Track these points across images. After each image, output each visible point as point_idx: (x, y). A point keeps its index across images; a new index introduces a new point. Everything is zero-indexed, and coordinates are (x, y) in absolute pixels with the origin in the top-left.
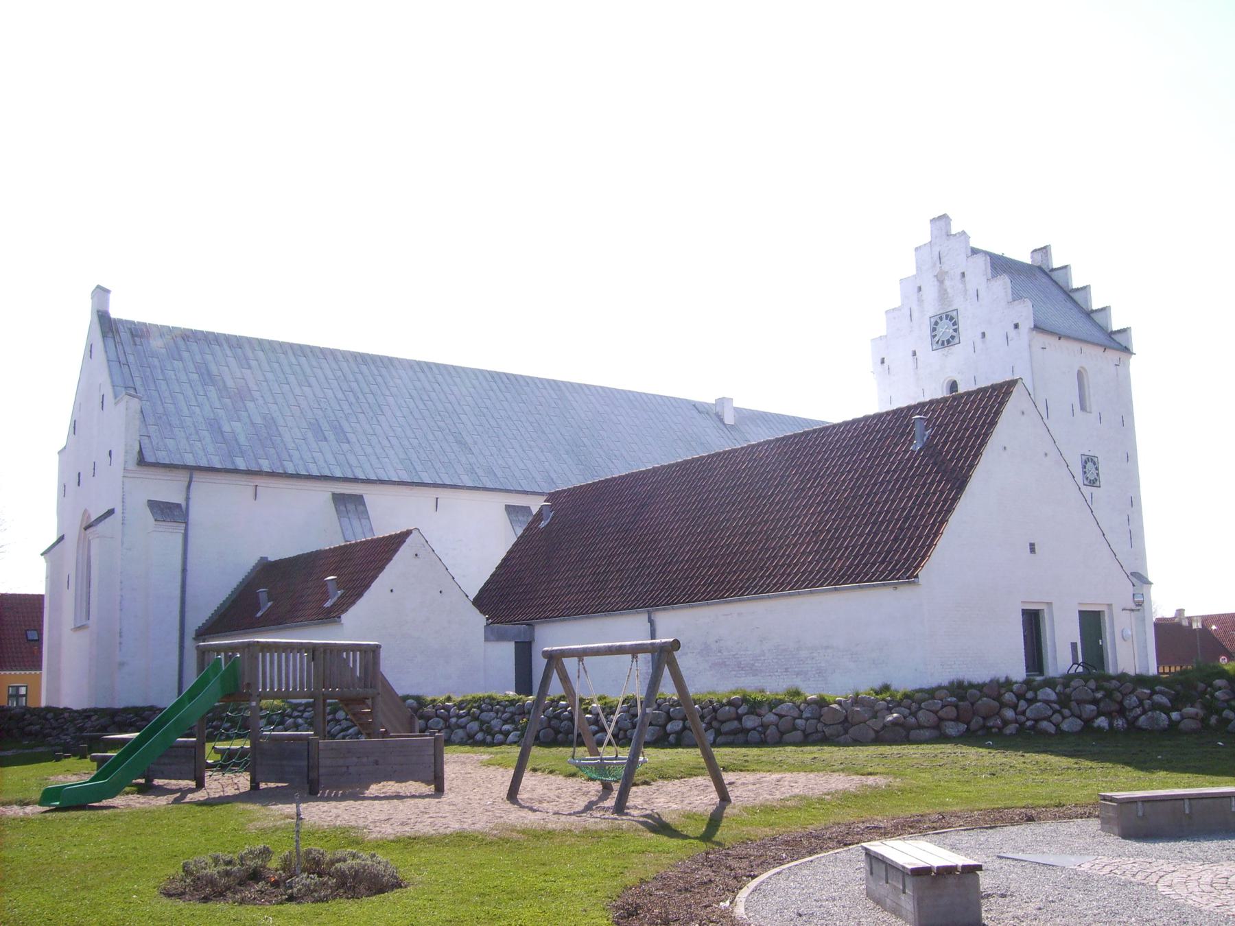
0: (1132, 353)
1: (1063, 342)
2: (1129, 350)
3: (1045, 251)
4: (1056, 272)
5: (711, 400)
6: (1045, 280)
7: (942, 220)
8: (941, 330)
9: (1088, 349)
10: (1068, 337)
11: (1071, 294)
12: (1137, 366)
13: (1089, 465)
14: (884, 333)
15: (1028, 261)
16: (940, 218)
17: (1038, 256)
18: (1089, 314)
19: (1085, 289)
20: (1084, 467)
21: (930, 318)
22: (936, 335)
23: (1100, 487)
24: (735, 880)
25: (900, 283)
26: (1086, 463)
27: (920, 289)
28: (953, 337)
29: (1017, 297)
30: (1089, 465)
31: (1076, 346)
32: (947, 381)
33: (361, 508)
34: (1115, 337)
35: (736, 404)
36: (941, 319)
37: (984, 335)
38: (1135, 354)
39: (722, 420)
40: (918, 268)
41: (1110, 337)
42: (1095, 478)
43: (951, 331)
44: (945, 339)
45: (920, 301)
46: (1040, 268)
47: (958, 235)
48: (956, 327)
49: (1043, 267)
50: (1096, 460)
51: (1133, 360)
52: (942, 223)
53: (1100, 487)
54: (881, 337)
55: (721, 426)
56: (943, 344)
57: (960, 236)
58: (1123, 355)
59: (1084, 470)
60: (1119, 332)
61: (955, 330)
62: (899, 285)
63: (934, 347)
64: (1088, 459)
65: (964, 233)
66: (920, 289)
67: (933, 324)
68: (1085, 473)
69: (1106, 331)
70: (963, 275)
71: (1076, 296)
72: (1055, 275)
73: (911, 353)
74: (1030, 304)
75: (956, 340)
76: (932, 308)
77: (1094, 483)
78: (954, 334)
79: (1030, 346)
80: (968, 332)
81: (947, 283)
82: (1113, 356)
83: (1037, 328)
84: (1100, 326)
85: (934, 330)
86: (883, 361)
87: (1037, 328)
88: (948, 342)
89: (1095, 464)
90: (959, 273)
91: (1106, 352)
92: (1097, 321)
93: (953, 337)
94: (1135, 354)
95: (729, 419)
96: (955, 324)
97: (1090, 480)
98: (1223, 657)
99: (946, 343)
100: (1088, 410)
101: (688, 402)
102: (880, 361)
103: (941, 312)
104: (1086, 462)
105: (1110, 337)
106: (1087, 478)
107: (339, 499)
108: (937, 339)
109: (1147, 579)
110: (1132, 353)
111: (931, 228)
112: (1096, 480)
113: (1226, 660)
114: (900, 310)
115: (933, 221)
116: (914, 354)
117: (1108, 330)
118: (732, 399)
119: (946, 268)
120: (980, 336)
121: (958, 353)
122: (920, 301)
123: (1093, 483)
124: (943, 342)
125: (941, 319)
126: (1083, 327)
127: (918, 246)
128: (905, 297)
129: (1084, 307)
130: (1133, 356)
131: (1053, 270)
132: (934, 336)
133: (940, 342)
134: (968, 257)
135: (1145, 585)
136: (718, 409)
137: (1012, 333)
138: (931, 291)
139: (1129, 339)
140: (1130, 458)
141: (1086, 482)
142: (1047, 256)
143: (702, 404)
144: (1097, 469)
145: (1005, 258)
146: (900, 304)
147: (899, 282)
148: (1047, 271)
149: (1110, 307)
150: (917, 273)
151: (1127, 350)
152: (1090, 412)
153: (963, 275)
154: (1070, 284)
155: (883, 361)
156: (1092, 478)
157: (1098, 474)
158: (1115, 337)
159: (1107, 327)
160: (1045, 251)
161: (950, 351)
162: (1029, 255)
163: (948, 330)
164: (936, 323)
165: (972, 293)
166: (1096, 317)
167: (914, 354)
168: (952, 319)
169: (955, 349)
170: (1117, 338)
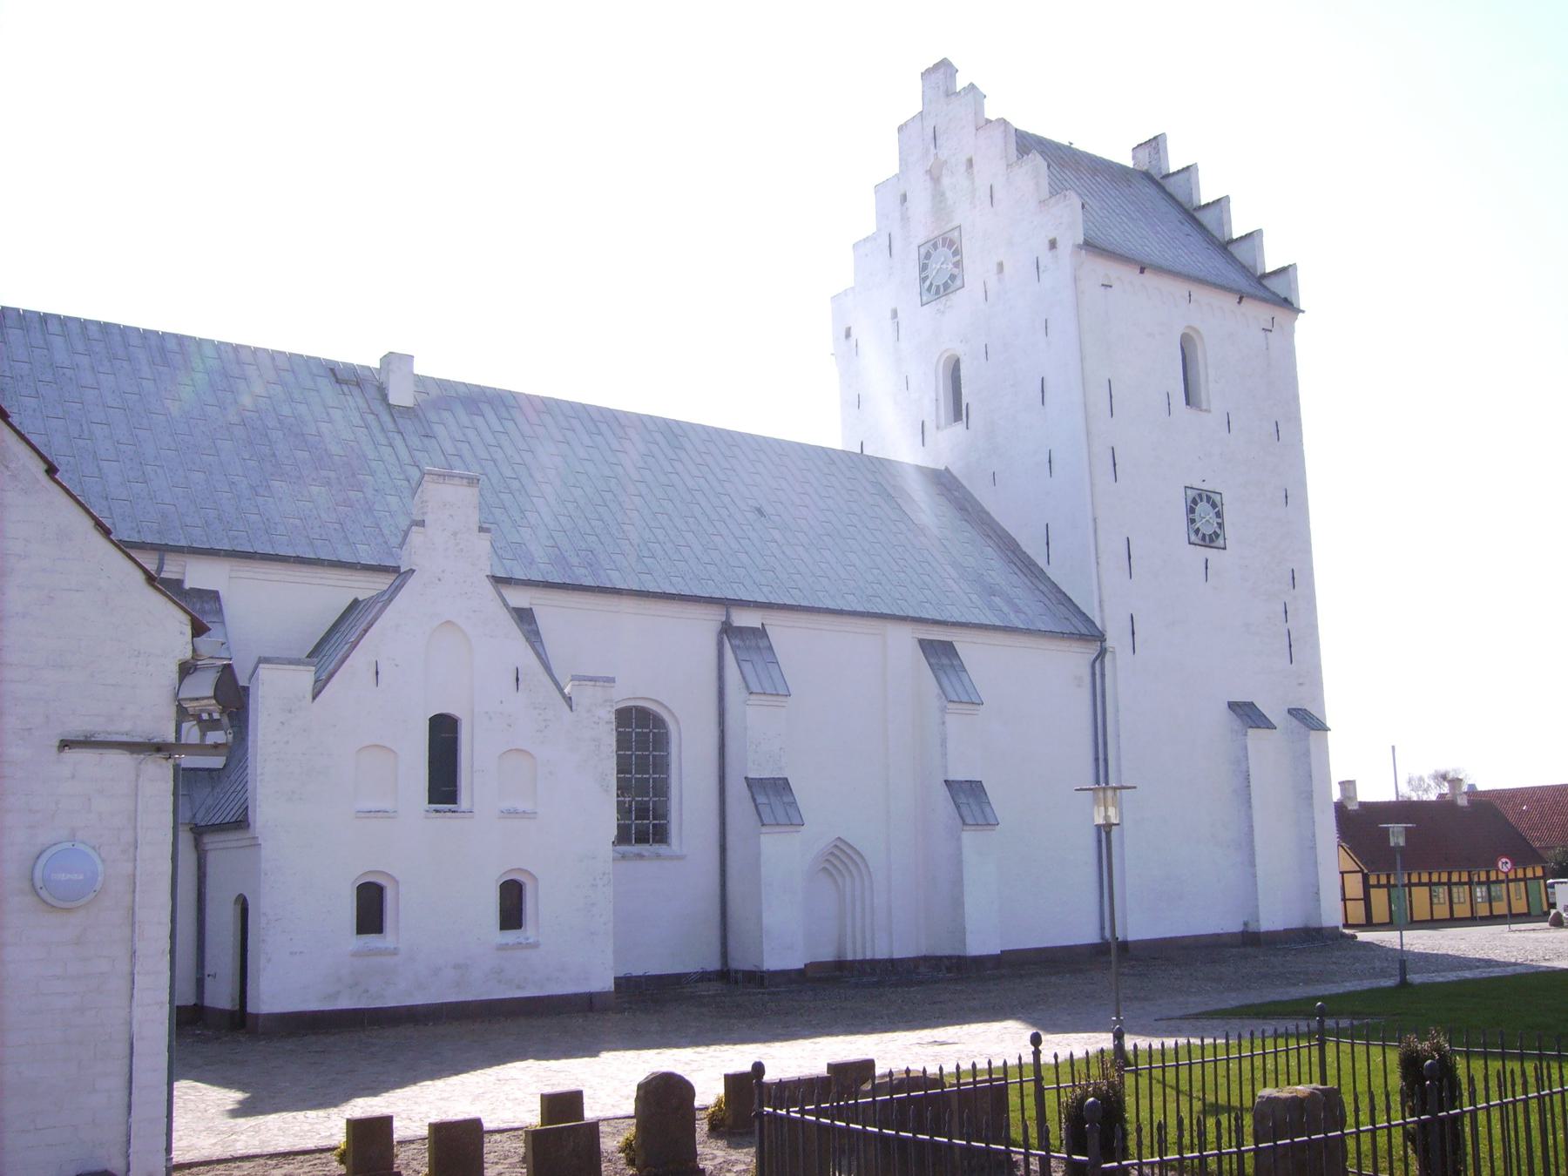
0: (1300, 311)
1: (1149, 279)
2: (1292, 304)
3: (1155, 145)
4: (1172, 180)
5: (368, 358)
6: (1151, 191)
7: (944, 68)
8: (934, 266)
9: (1203, 295)
10: (1161, 270)
11: (1198, 215)
12: (1304, 329)
13: (1203, 507)
14: (853, 285)
15: (1129, 163)
16: (937, 67)
17: (1144, 154)
18: (1225, 247)
19: (1221, 204)
20: (1192, 510)
21: (919, 247)
22: (927, 277)
23: (1225, 548)
24: (1249, 960)
25: (876, 193)
26: (1196, 504)
27: (904, 198)
28: (953, 277)
29: (1056, 190)
30: (1203, 507)
31: (1179, 289)
32: (946, 355)
33: (762, 644)
34: (1266, 282)
35: (420, 369)
36: (935, 246)
37: (1000, 266)
38: (1303, 312)
39: (385, 398)
40: (903, 161)
41: (1261, 284)
42: (1215, 532)
43: (950, 266)
44: (941, 283)
45: (905, 219)
46: (1147, 175)
47: (962, 93)
48: (958, 258)
49: (1153, 172)
50: (1217, 498)
51: (1301, 323)
52: (940, 75)
53: (1225, 548)
54: (846, 290)
55: (379, 408)
56: (937, 292)
57: (966, 94)
58: (1280, 314)
59: (1191, 516)
60: (1275, 273)
61: (958, 264)
62: (874, 196)
63: (925, 299)
64: (1200, 495)
65: (972, 87)
66: (904, 198)
67: (922, 257)
68: (1193, 521)
69: (1253, 275)
70: (970, 163)
71: (1204, 217)
72: (1170, 185)
73: (889, 315)
74: (1077, 202)
75: (958, 282)
76: (922, 230)
77: (1212, 540)
78: (956, 271)
79: (1076, 280)
80: (977, 269)
81: (946, 181)
82: (1257, 312)
83: (1090, 246)
84: (1243, 267)
85: (924, 268)
86: (848, 334)
87: (1090, 246)
88: (946, 286)
89: (1214, 505)
90: (964, 159)
91: (1242, 304)
92: (1238, 258)
93: (953, 277)
94: (1303, 312)
95: (401, 396)
96: (956, 253)
97: (1204, 535)
98: (1504, 860)
99: (942, 289)
100: (1204, 407)
101: (317, 361)
102: (844, 334)
103: (936, 233)
104: (1194, 502)
105: (1261, 284)
106: (1197, 532)
107: (927, 647)
108: (928, 283)
109: (1325, 725)
110: (1300, 311)
111: (923, 86)
112: (1217, 536)
113: (1509, 865)
114: (875, 239)
115: (926, 74)
116: (895, 314)
117: (1256, 271)
118: (413, 357)
119: (944, 154)
120: (995, 268)
121: (964, 302)
122: (905, 219)
123: (1210, 540)
124: (938, 287)
125: (935, 246)
126: (1212, 264)
127: (902, 123)
128: (882, 215)
129: (1216, 234)
130: (1300, 315)
131: (1168, 176)
132: (923, 280)
133: (934, 288)
134: (977, 130)
135: (1312, 732)
136: (383, 378)
137: (1046, 257)
138: (921, 203)
139: (1292, 285)
140: (1292, 497)
141: (1193, 538)
142: (1158, 152)
143: (351, 368)
144: (1219, 515)
145: (1073, 149)
146: (875, 230)
147: (873, 191)
148: (1158, 178)
149: (1227, 197)
150: (901, 171)
151: (1287, 304)
152: (1208, 411)
153: (970, 163)
154: (1194, 197)
155: (848, 334)
156: (1209, 531)
157: (1221, 525)
158: (1266, 282)
159: (1255, 267)
160: (1155, 145)
161: (948, 303)
162: (1130, 154)
163: (944, 266)
164: (928, 256)
165: (983, 193)
166: (1239, 252)
167: (895, 314)
168: (951, 243)
169: (958, 298)
170: (1272, 284)
